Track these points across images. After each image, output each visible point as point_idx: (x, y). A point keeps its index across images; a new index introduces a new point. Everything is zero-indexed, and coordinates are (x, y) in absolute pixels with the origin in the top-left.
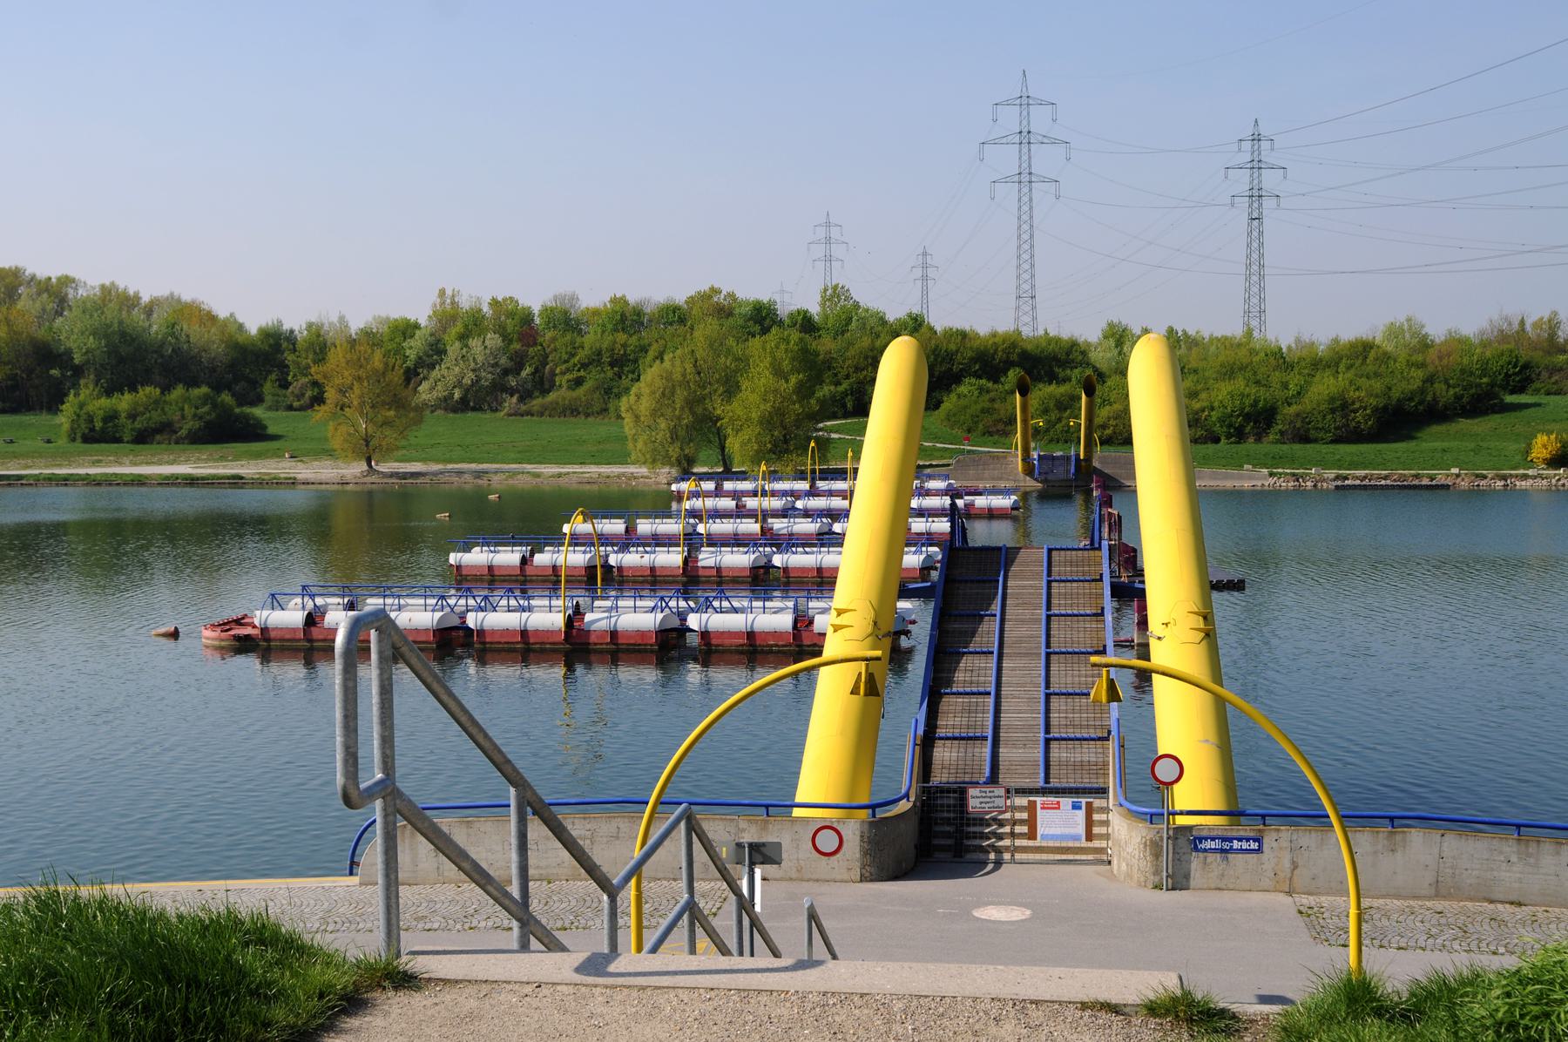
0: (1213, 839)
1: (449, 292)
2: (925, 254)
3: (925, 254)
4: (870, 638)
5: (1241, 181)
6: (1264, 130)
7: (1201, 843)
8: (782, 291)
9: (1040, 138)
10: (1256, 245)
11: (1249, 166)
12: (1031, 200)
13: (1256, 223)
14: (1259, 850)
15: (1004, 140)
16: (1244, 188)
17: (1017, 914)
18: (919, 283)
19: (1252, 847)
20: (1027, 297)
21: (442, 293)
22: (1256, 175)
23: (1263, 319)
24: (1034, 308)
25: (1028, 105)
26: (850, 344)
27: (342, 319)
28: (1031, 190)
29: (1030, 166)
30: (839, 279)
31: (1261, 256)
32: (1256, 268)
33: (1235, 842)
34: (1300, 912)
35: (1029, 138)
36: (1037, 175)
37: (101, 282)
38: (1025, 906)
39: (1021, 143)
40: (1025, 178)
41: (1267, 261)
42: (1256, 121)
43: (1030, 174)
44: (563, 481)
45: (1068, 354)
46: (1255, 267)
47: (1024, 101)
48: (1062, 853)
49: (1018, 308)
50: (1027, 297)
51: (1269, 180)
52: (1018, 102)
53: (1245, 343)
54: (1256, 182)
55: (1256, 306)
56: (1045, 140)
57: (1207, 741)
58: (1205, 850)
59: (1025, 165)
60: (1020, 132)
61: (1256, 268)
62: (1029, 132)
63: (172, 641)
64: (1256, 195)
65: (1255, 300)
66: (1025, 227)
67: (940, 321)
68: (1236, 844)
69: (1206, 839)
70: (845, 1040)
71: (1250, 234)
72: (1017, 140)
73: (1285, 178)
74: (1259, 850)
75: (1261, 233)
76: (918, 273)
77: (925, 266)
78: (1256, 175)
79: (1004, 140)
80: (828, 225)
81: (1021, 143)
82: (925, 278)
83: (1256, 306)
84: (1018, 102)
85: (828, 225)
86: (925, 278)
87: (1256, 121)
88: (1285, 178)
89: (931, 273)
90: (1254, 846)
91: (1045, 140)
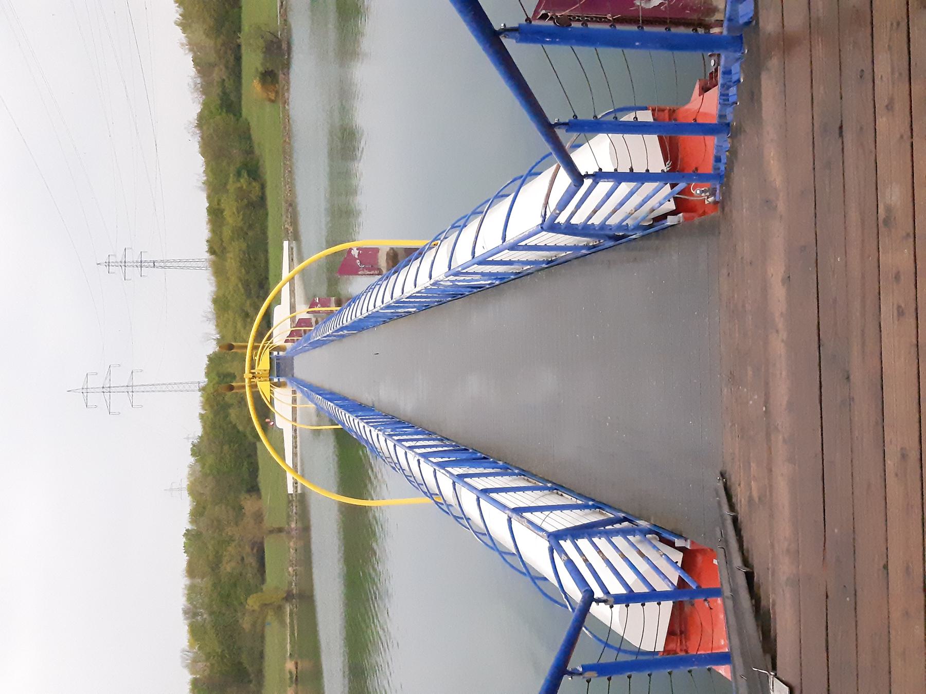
13: (152, 264)
15: (109, 407)
22: (146, 264)
52: (85, 394)
75: (162, 261)
78: (146, 264)
79: (109, 407)
84: (85, 394)
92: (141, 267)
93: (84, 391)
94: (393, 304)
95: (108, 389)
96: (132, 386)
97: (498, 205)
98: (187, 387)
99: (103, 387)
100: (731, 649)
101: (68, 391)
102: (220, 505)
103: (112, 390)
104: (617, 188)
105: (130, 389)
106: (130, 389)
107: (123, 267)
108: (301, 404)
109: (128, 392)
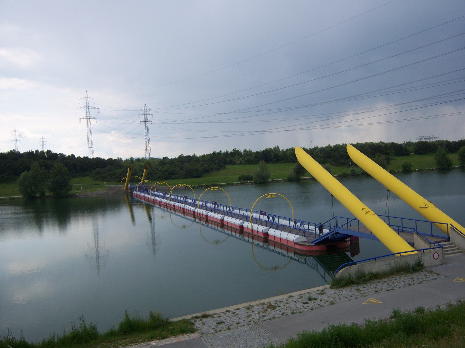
5: (142, 118)
6: (147, 106)
11: (144, 114)
13: (147, 128)
18: (42, 146)
22: (146, 116)
34: (388, 290)
36: (92, 117)
37: (231, 151)
39: (87, 109)
40: (88, 117)
45: (460, 160)
48: (453, 249)
63: (363, 208)
64: (146, 121)
70: (240, 347)
72: (86, 108)
73: (153, 117)
76: (41, 143)
77: (43, 142)
78: (146, 116)
79: (82, 108)
80: (15, 131)
81: (87, 109)
88: (153, 117)
89: (45, 143)
91: (93, 108)
101: (86, 91)
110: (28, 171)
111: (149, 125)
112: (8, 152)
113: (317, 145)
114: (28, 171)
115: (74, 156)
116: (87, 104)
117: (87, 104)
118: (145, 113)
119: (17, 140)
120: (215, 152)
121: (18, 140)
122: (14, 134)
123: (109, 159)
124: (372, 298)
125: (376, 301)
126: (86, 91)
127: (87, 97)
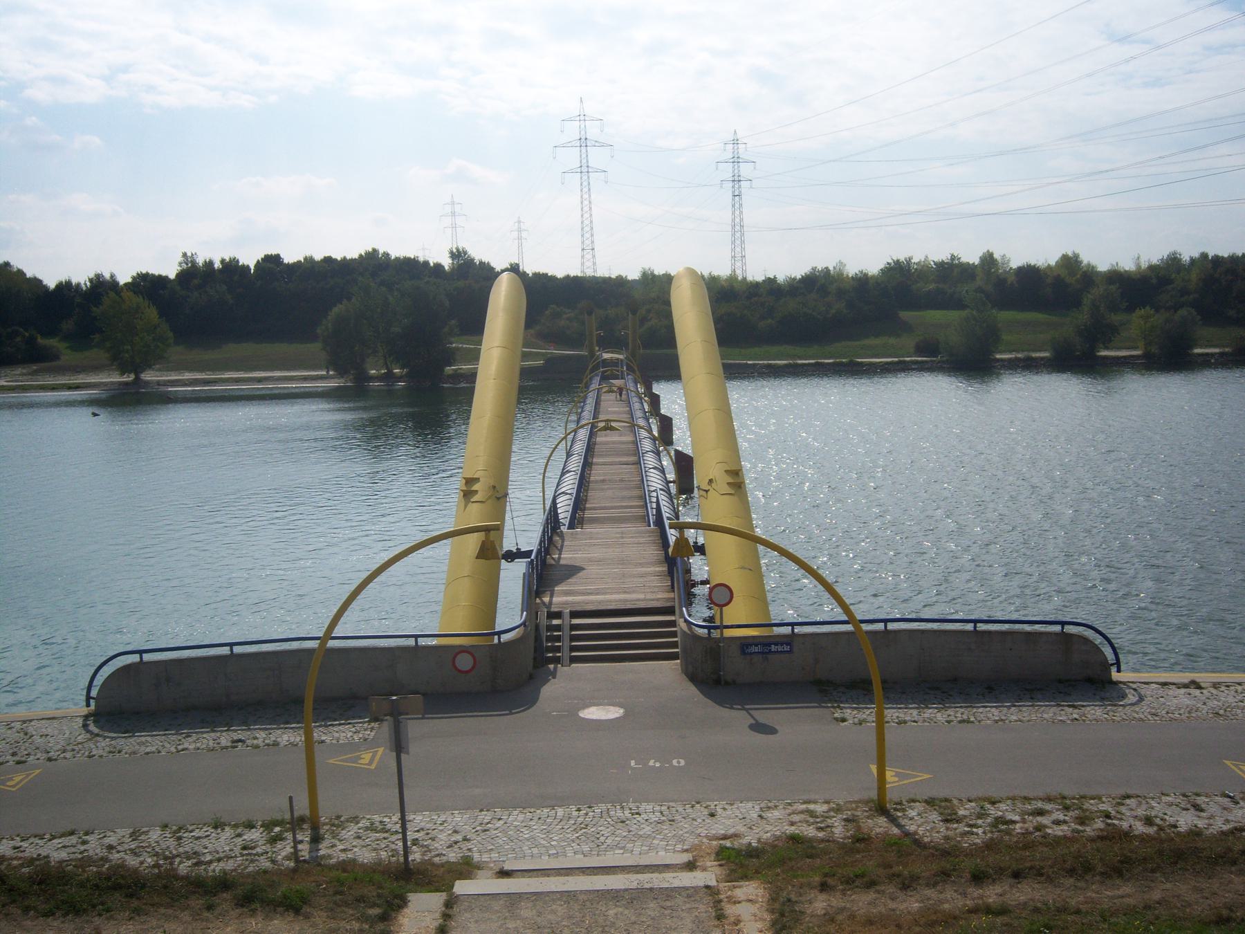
0: (756, 645)
1: (189, 254)
2: (519, 222)
3: (519, 222)
4: (490, 501)
7: (747, 648)
8: (424, 249)
9: (594, 143)
10: (736, 212)
11: (731, 161)
12: (589, 184)
13: (737, 198)
14: (790, 651)
15: (569, 145)
16: (729, 176)
17: (614, 713)
19: (785, 649)
20: (588, 248)
21: (185, 255)
22: (736, 167)
23: (744, 261)
24: (594, 256)
25: (585, 120)
26: (801, 902)
27: (112, 276)
28: (588, 177)
29: (587, 162)
30: (463, 244)
31: (741, 220)
32: (738, 229)
33: (773, 646)
35: (586, 143)
38: (621, 706)
39: (581, 146)
41: (746, 222)
42: (735, 132)
43: (588, 167)
44: (327, 382)
46: (738, 228)
47: (582, 118)
49: (583, 257)
50: (588, 248)
51: (745, 170)
52: (578, 118)
53: (732, 278)
54: (736, 171)
55: (738, 255)
56: (597, 144)
57: (743, 568)
58: (751, 654)
59: (584, 161)
60: (580, 139)
61: (738, 229)
62: (586, 139)
64: (736, 180)
65: (738, 249)
66: (586, 203)
67: (530, 268)
68: (773, 648)
69: (751, 645)
71: (733, 206)
74: (790, 652)
75: (741, 205)
76: (515, 234)
77: (520, 230)
78: (736, 167)
79: (569, 145)
80: (453, 203)
82: (520, 238)
83: (738, 255)
84: (578, 118)
85: (453, 203)
86: (520, 238)
87: (735, 132)
88: (717, 169)
89: (524, 235)
90: (787, 648)
91: (597, 144)
92: (734, 181)
93: (582, 118)
94: (637, 372)
95: (584, 145)
96: (588, 172)
97: (710, 313)
98: (587, 215)
99: (586, 139)
100: (709, 576)
101: (581, 98)
102: (877, 802)
103: (584, 149)
104: (646, 866)
105: (585, 170)
106: (585, 170)
107: (732, 142)
108: (618, 367)
109: (581, 167)
110: (349, 299)
111: (743, 191)
112: (361, 256)
113: (1077, 252)
114: (349, 299)
115: (238, 261)
116: (583, 133)
117: (583, 133)
118: (734, 157)
119: (457, 226)
120: (306, 257)
121: (461, 227)
122: (450, 211)
123: (23, 272)
124: (14, 789)
125: (361, 764)
126: (581, 98)
127: (582, 113)
